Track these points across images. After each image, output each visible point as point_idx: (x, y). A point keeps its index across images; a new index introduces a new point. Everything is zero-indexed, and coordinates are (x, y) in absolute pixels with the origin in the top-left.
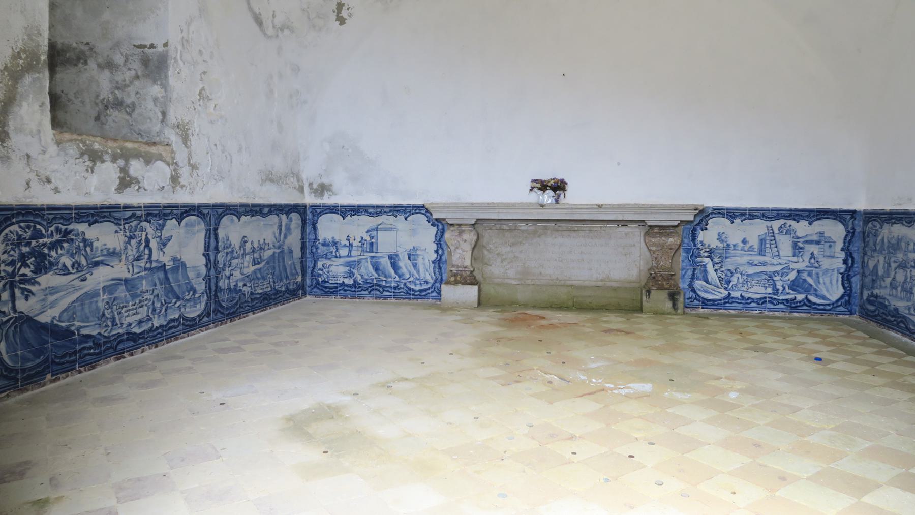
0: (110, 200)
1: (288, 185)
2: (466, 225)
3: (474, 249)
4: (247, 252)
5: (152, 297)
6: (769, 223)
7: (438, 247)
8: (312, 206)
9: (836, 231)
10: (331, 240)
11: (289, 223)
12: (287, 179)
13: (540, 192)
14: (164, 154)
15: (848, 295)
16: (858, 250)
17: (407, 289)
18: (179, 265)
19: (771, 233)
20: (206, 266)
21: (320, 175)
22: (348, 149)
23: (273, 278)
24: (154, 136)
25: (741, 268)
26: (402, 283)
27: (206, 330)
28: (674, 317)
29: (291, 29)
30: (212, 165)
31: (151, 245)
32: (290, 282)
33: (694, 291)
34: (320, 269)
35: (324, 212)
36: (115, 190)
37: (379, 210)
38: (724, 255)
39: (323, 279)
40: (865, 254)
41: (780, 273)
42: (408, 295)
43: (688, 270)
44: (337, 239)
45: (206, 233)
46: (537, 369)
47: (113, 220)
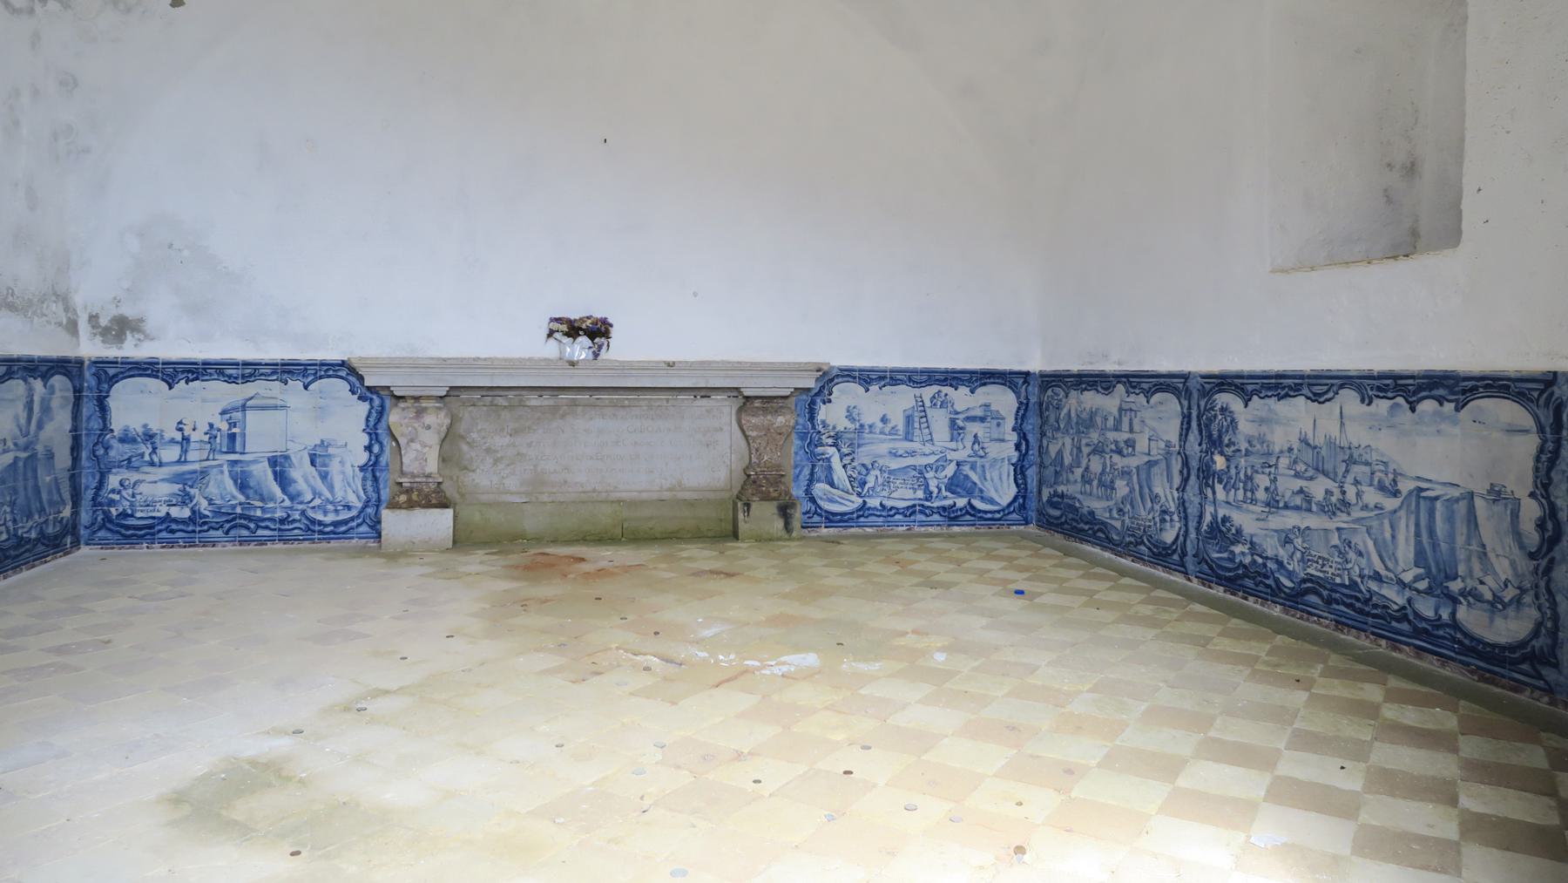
1: (45, 318)
3: (443, 440)
6: (918, 392)
7: (371, 440)
8: (95, 362)
9: (1004, 401)
11: (48, 396)
12: (45, 306)
13: (566, 340)
15: (1022, 497)
16: (1033, 429)
17: (306, 522)
19: (920, 406)
21: (115, 298)
23: (12, 512)
25: (881, 462)
26: (297, 510)
28: (787, 543)
32: (47, 520)
33: (813, 500)
34: (113, 491)
35: (127, 374)
38: (856, 442)
39: (121, 509)
40: (1043, 434)
41: (934, 468)
42: (309, 533)
44: (154, 427)
46: (618, 648)
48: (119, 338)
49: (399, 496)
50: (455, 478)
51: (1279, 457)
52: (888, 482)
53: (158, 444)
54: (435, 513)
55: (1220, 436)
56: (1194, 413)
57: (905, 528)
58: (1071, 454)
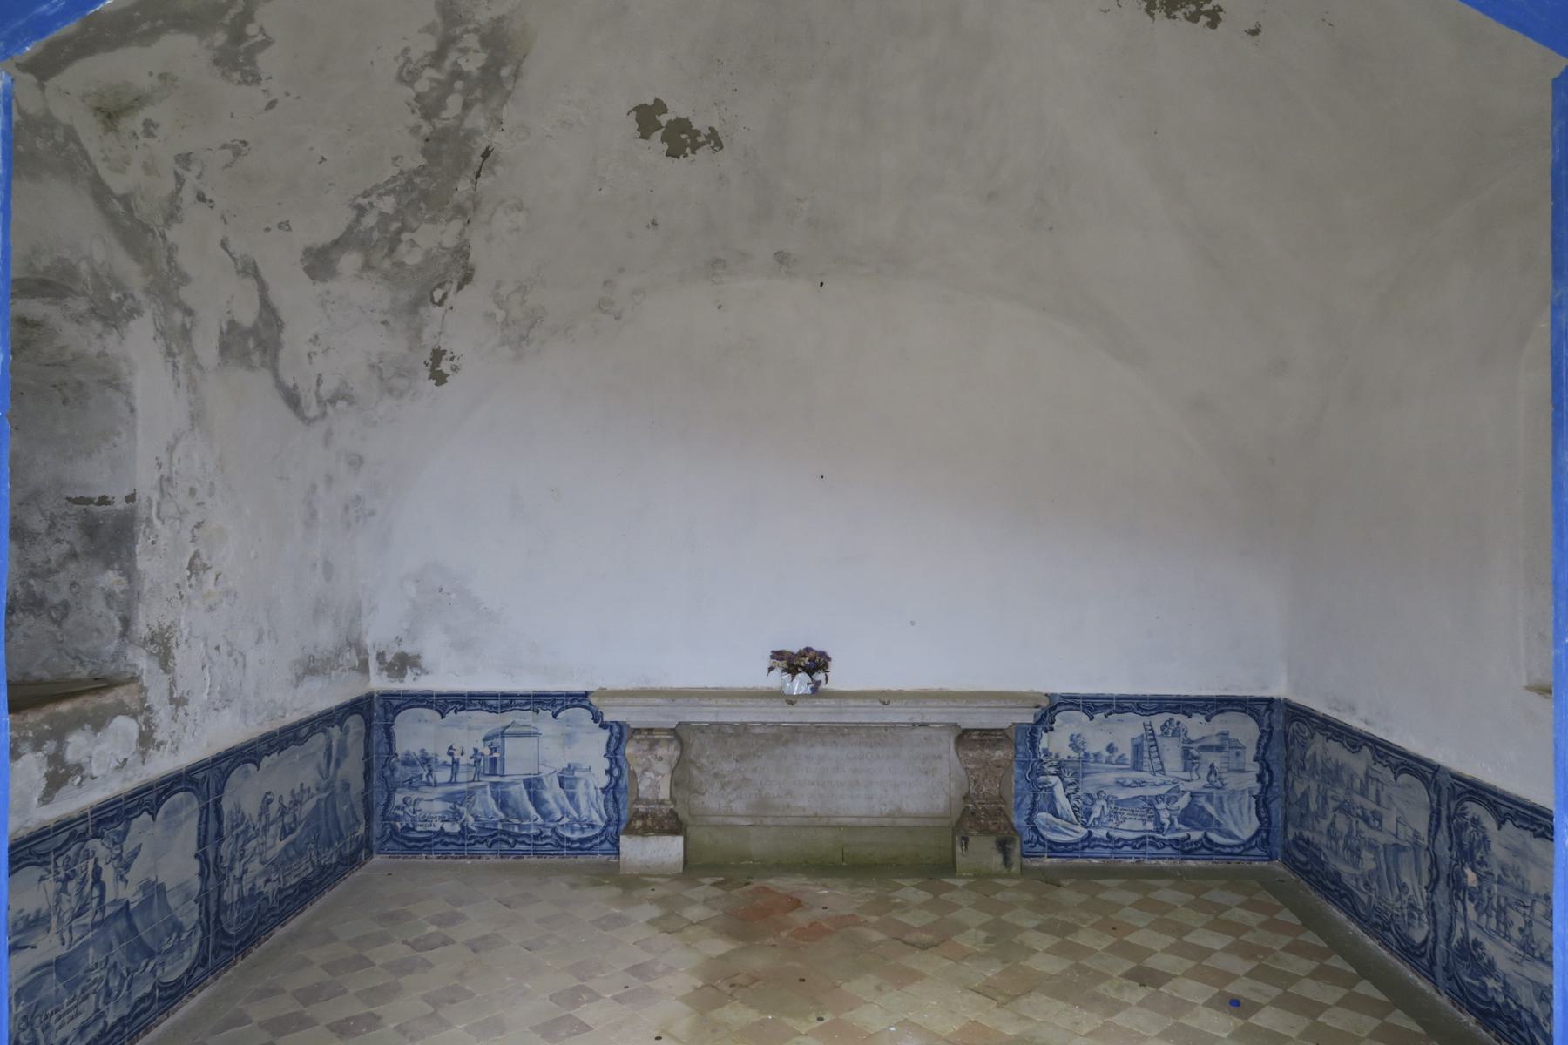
0: (29, 823)
2: (661, 730)
4: (271, 820)
5: (104, 973)
6: (1146, 720)
9: (1245, 730)
10: (418, 754)
14: (127, 700)
16: (1278, 759)
17: (556, 838)
18: (154, 891)
19: (1150, 735)
20: (201, 874)
21: (397, 638)
22: (449, 594)
24: (104, 661)
25: (1107, 792)
27: (200, 992)
29: (350, 399)
30: (210, 686)
31: (103, 878)
33: (1035, 829)
34: (398, 808)
35: (407, 705)
36: (39, 800)
37: (506, 701)
39: (404, 824)
40: (1288, 769)
42: (559, 848)
43: (1025, 796)
44: (430, 751)
45: (202, 815)
47: (35, 860)
48: (401, 674)
49: (635, 821)
50: (686, 801)
51: (1534, 900)
52: (1116, 813)
53: (433, 767)
54: (669, 838)
55: (1471, 851)
56: (1444, 813)
57: (1133, 860)
58: (1317, 801)
